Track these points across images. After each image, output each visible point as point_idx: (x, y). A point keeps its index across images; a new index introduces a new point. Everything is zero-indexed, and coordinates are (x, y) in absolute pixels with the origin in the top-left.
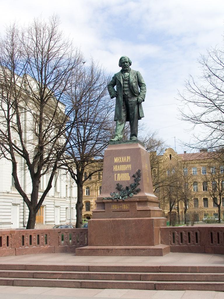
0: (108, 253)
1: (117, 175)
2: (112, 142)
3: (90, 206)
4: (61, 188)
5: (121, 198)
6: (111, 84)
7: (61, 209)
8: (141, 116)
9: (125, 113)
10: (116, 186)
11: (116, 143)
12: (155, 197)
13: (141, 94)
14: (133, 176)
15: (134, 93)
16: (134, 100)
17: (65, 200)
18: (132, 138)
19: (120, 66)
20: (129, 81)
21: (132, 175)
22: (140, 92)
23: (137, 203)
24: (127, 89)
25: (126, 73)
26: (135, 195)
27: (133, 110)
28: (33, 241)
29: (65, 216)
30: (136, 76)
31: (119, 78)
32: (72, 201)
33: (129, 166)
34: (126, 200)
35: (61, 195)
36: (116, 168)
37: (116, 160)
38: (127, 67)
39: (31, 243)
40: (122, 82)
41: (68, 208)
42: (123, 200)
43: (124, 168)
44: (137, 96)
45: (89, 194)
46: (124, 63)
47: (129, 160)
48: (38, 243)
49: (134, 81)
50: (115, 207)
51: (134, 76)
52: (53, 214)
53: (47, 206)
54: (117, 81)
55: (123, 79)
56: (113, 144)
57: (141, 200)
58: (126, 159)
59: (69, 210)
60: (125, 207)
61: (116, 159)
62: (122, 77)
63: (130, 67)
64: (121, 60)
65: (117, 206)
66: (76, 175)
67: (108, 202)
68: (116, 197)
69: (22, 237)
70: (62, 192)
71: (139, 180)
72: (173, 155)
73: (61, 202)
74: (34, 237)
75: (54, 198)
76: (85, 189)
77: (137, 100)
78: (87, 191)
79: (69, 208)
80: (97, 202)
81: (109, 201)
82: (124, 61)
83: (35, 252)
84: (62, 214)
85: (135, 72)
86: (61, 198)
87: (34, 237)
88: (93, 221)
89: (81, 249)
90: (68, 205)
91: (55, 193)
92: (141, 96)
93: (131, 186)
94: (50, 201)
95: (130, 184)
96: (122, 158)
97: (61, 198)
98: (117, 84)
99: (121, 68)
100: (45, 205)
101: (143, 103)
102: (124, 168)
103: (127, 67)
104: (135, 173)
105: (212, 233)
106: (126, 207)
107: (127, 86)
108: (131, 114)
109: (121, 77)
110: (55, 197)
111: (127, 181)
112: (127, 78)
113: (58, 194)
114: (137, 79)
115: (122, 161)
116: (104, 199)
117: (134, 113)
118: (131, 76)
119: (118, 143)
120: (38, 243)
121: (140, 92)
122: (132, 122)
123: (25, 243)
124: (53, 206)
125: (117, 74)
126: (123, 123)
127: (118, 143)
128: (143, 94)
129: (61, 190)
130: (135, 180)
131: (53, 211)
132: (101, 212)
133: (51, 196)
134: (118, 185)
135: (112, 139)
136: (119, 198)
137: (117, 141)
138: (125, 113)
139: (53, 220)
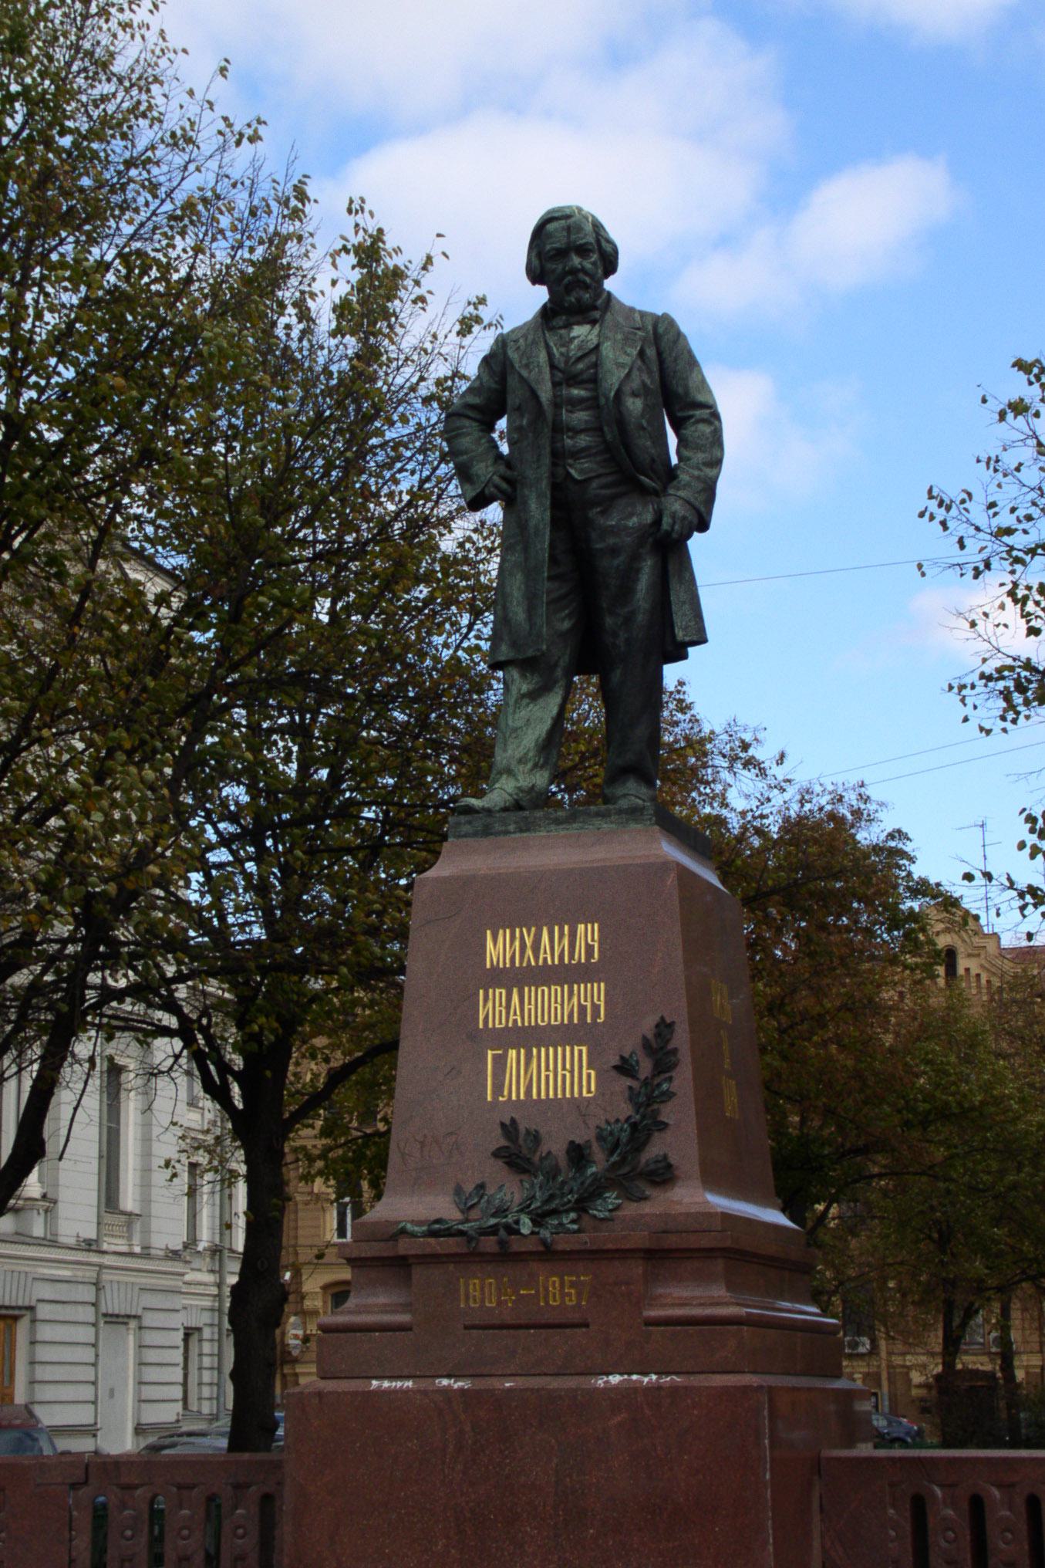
1: (500, 1062)
2: (468, 818)
5: (526, 1226)
6: (472, 407)
7: (150, 1338)
8: (680, 635)
9: (569, 616)
12: (793, 1230)
13: (684, 477)
14: (616, 1068)
17: (178, 1267)
19: (536, 275)
20: (594, 381)
21: (615, 1060)
22: (674, 460)
23: (637, 1269)
24: (583, 440)
25: (580, 331)
26: (631, 1209)
27: (626, 590)
29: (177, 1392)
30: (651, 352)
31: (527, 366)
33: (594, 994)
34: (563, 1244)
35: (146, 1231)
37: (498, 949)
38: (587, 287)
40: (545, 393)
41: (199, 1329)
42: (543, 1242)
44: (656, 493)
46: (562, 254)
47: (589, 949)
49: (635, 384)
51: (635, 352)
52: (88, 1374)
53: (44, 1311)
54: (512, 382)
55: (553, 367)
56: (475, 834)
57: (672, 1241)
58: (566, 941)
59: (207, 1348)
62: (550, 355)
63: (610, 284)
64: (540, 233)
65: (499, 1289)
66: (238, 1077)
68: (493, 1221)
70: (153, 1213)
71: (663, 1093)
72: (969, 956)
75: (94, 1258)
77: (658, 521)
79: (207, 1333)
80: (355, 1254)
81: (439, 1250)
84: (151, 1374)
85: (639, 324)
86: (146, 1254)
90: (203, 1309)
91: (109, 1218)
92: (681, 493)
95: (593, 1123)
97: (146, 1254)
98: (509, 407)
99: (541, 295)
100: (31, 1309)
101: (696, 543)
103: (587, 287)
104: (630, 1045)
106: (563, 1295)
108: (609, 621)
109: (543, 357)
110: (105, 1247)
111: (578, 1106)
112: (580, 366)
113: (129, 1225)
114: (655, 368)
115: (536, 958)
116: (403, 1232)
117: (633, 613)
118: (607, 349)
119: (512, 828)
121: (674, 460)
122: (616, 676)
125: (514, 337)
126: (556, 682)
127: (512, 828)
128: (698, 478)
129: (146, 1200)
130: (632, 1095)
131: (88, 1355)
133: (72, 1241)
134: (510, 1129)
135: (473, 802)
136: (513, 1230)
137: (505, 809)
138: (569, 616)
139: (82, 1416)
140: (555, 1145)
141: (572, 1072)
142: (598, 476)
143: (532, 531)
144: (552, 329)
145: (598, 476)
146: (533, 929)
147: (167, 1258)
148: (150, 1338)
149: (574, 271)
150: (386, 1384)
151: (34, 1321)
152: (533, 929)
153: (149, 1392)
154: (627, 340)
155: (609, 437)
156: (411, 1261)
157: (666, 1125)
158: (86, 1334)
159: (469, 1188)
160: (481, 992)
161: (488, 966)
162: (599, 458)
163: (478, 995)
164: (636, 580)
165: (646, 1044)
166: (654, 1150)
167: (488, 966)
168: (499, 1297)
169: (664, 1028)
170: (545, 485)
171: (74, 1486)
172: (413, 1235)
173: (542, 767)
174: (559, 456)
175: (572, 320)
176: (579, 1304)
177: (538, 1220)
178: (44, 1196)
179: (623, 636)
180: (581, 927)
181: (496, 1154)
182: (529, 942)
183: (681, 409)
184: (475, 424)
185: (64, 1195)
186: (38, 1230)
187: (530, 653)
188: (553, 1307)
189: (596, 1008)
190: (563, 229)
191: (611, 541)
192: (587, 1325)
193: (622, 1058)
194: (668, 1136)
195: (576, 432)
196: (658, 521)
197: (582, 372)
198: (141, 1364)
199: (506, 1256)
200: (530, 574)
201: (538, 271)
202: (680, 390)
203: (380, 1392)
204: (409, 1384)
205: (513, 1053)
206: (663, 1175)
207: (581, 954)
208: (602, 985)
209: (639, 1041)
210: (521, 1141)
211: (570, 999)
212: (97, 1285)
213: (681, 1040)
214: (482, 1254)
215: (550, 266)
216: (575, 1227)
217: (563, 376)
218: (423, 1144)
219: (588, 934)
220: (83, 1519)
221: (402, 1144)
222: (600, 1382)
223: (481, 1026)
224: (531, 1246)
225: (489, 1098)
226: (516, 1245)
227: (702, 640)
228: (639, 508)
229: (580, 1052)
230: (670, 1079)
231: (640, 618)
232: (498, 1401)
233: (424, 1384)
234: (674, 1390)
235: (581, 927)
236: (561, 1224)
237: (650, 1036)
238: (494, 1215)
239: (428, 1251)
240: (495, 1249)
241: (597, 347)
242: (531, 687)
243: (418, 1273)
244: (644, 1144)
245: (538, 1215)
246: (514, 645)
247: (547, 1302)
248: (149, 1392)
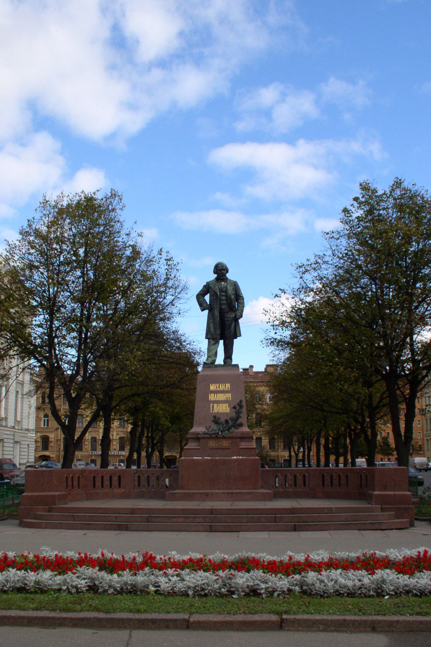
0: (207, 497)
1: (213, 406)
3: (48, 444)
4: (22, 415)
5: (220, 433)
7: (22, 446)
10: (213, 419)
15: (232, 309)
16: (232, 316)
18: (227, 361)
19: (215, 273)
21: (233, 406)
23: (239, 440)
24: (224, 302)
25: (223, 283)
26: (236, 430)
27: (230, 328)
28: (97, 485)
33: (229, 395)
35: (22, 425)
36: (212, 397)
37: (212, 387)
39: (102, 487)
40: (218, 294)
42: (224, 436)
43: (221, 397)
45: (48, 425)
46: (221, 270)
47: (228, 388)
48: (111, 486)
49: (232, 293)
50: (212, 443)
53: (5, 440)
57: (244, 436)
60: (225, 443)
67: (204, 438)
69: (118, 478)
73: (22, 435)
74: (106, 478)
75: (14, 430)
76: (43, 416)
78: (44, 420)
82: (221, 268)
83: (106, 496)
84: (22, 453)
86: (21, 430)
87: (106, 478)
88: (185, 459)
89: (172, 493)
94: (9, 433)
96: (219, 386)
99: (216, 275)
101: (240, 321)
102: (221, 397)
104: (235, 404)
105: (323, 476)
107: (224, 298)
108: (226, 332)
109: (217, 287)
111: (226, 413)
113: (19, 423)
116: (199, 434)
118: (228, 287)
120: (111, 486)
122: (227, 341)
123: (104, 485)
124: (12, 441)
129: (22, 419)
130: (236, 412)
132: (195, 449)
133: (10, 426)
134: (215, 417)
136: (218, 433)
140: (223, 420)
144: (218, 282)
147: (25, 430)
148: (22, 446)
149: (223, 273)
150: (196, 458)
151: (20, 444)
153: (22, 457)
154: (231, 285)
157: (241, 417)
158: (12, 445)
159: (208, 426)
165: (238, 404)
166: (239, 421)
169: (241, 401)
170: (218, 309)
171: (135, 474)
172: (201, 434)
174: (221, 304)
177: (222, 432)
178: (5, 417)
179: (229, 335)
181: (213, 421)
185: (9, 417)
186: (4, 424)
187: (215, 337)
189: (229, 398)
191: (228, 319)
192: (230, 449)
194: (242, 419)
195: (223, 300)
196: (236, 316)
198: (20, 451)
199: (217, 438)
200: (214, 322)
203: (195, 459)
204: (200, 458)
206: (241, 425)
212: (14, 435)
213: (244, 403)
215: (218, 272)
217: (221, 291)
219: (228, 385)
220: (136, 479)
222: (233, 458)
224: (221, 436)
226: (219, 436)
227: (240, 336)
232: (216, 461)
233: (203, 458)
234: (245, 459)
241: (226, 286)
243: (201, 440)
246: (211, 335)
248: (22, 457)
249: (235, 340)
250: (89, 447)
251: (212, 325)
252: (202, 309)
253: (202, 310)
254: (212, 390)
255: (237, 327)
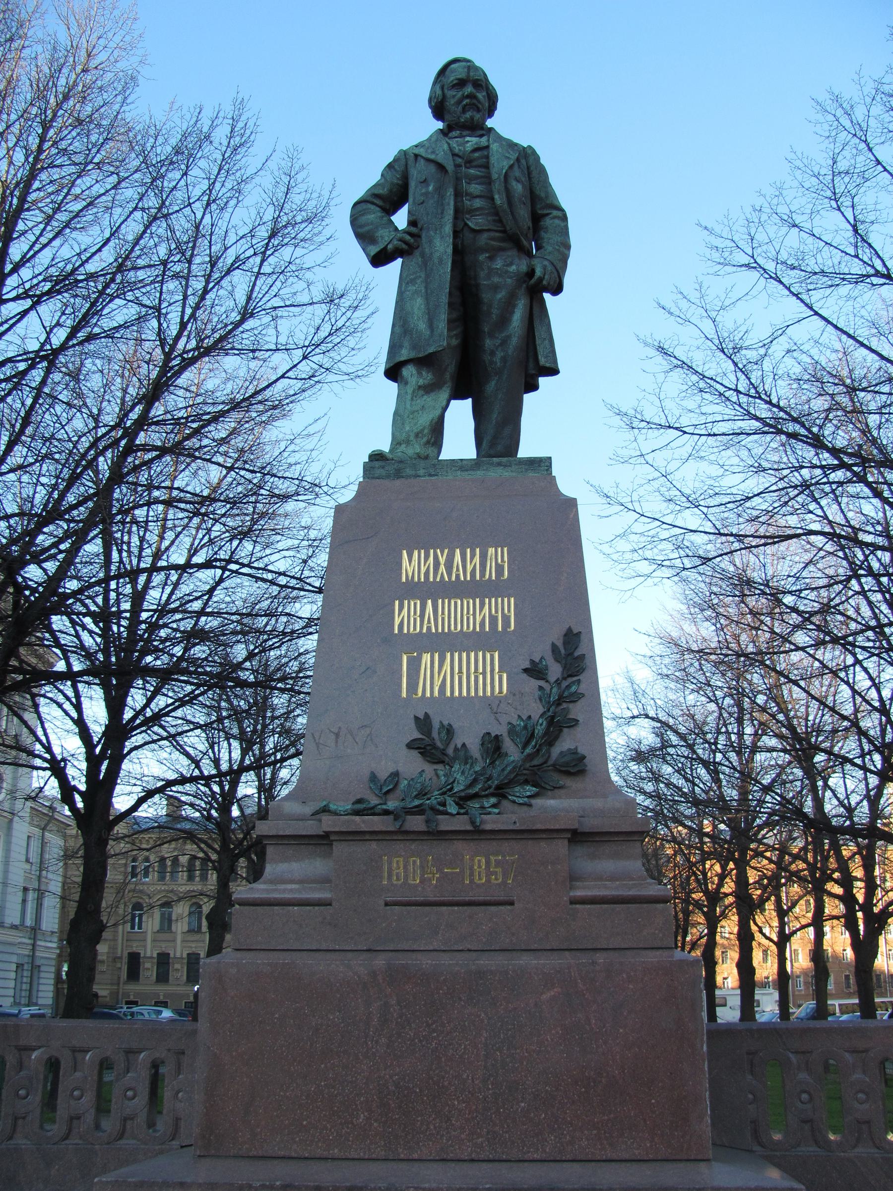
11: (409, 471)
14: (526, 670)
21: (527, 665)
24: (478, 203)
27: (504, 320)
32: (39, 943)
47: (499, 569)
56: (388, 477)
61: (410, 561)
65: (422, 867)
66: (81, 793)
68: (417, 802)
71: (572, 695)
79: (26, 967)
81: (364, 828)
90: (25, 955)
93: (512, 731)
95: (504, 719)
104: (541, 651)
106: (489, 874)
108: (488, 343)
111: (492, 705)
115: (450, 574)
117: (509, 337)
119: (421, 472)
126: (445, 383)
134: (423, 723)
141: (484, 673)
142: (489, 230)
143: (436, 261)
145: (489, 230)
146: (446, 551)
152: (446, 551)
155: (498, 202)
156: (332, 838)
160: (397, 602)
161: (404, 580)
162: (490, 218)
163: (394, 605)
164: (512, 313)
165: (554, 648)
167: (404, 580)
168: (422, 876)
173: (433, 445)
175: (465, 133)
176: (504, 883)
179: (499, 354)
180: (491, 551)
181: (410, 746)
182: (442, 560)
183: (541, 209)
184: (378, 209)
188: (478, 886)
189: (506, 619)
190: (465, 67)
191: (496, 280)
192: (512, 903)
193: (532, 661)
197: (475, 160)
201: (440, 98)
202: (543, 195)
205: (426, 658)
207: (491, 572)
208: (512, 600)
209: (549, 648)
210: (435, 734)
211: (481, 611)
214: (407, 832)
216: (496, 811)
218: (337, 735)
221: (317, 736)
223: (396, 631)
225: (404, 695)
226: (445, 824)
228: (516, 261)
229: (415, 604)
230: (579, 681)
231: (514, 341)
235: (491, 551)
236: (483, 807)
237: (559, 644)
238: (416, 797)
239: (352, 828)
240: (423, 827)
242: (426, 382)
244: (557, 738)
245: (461, 798)
247: (472, 881)
249: (526, 397)
250: (182, 976)
251: (418, 305)
252: (374, 250)
253: (379, 260)
254: (410, 583)
255: (537, 323)
